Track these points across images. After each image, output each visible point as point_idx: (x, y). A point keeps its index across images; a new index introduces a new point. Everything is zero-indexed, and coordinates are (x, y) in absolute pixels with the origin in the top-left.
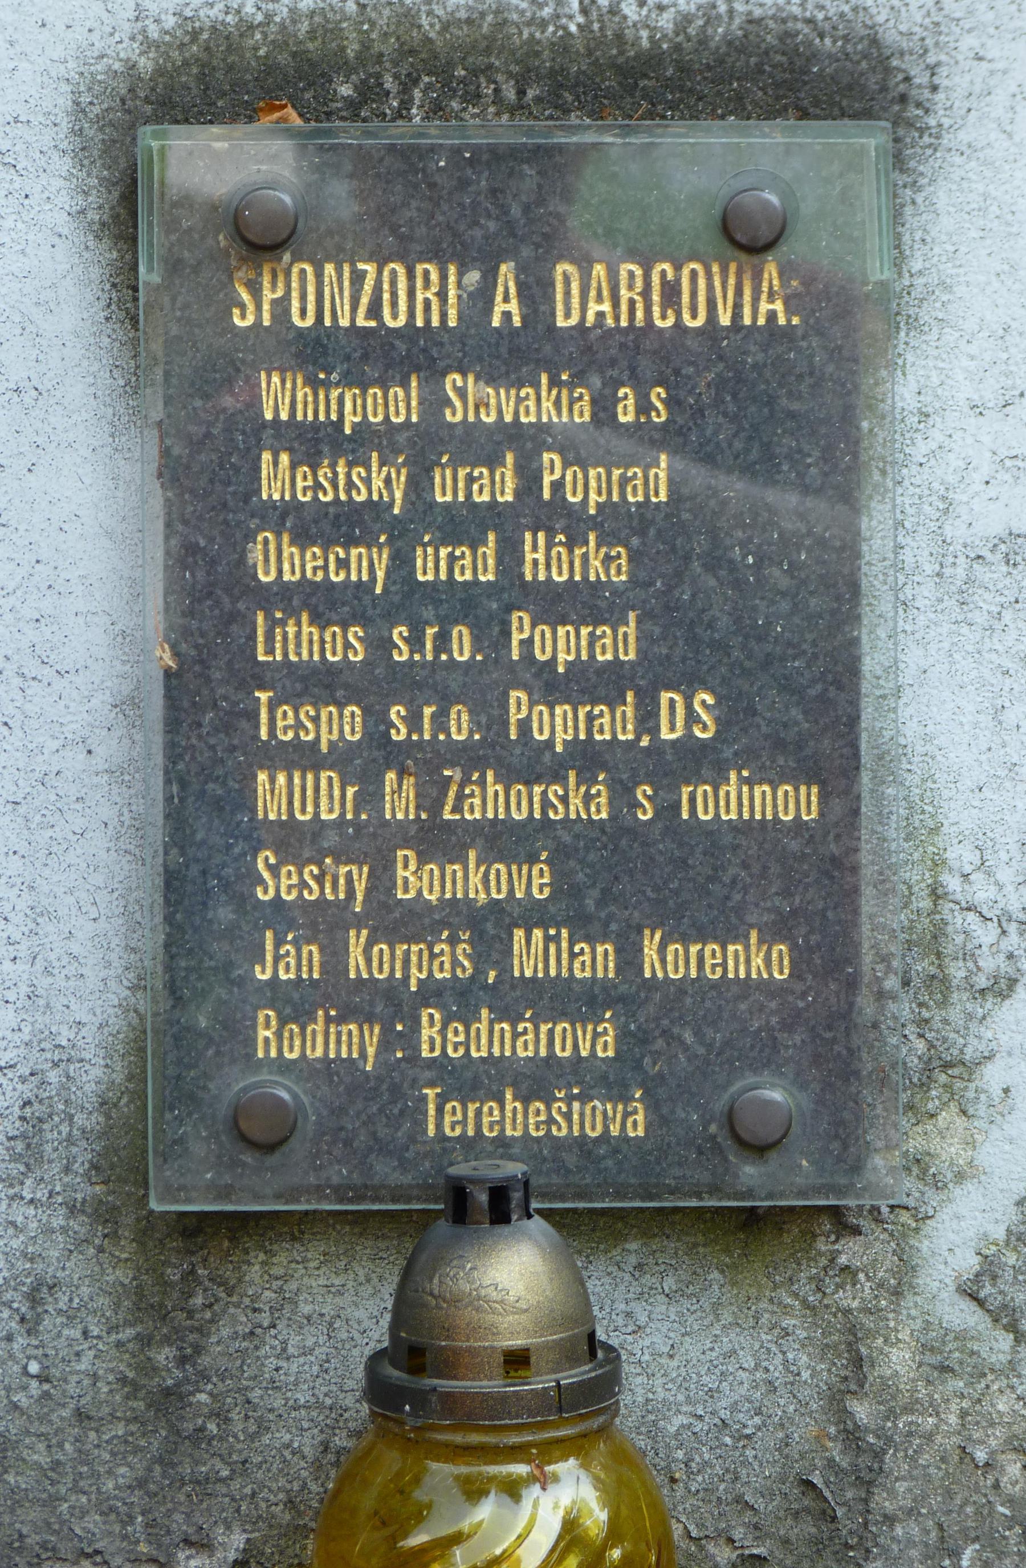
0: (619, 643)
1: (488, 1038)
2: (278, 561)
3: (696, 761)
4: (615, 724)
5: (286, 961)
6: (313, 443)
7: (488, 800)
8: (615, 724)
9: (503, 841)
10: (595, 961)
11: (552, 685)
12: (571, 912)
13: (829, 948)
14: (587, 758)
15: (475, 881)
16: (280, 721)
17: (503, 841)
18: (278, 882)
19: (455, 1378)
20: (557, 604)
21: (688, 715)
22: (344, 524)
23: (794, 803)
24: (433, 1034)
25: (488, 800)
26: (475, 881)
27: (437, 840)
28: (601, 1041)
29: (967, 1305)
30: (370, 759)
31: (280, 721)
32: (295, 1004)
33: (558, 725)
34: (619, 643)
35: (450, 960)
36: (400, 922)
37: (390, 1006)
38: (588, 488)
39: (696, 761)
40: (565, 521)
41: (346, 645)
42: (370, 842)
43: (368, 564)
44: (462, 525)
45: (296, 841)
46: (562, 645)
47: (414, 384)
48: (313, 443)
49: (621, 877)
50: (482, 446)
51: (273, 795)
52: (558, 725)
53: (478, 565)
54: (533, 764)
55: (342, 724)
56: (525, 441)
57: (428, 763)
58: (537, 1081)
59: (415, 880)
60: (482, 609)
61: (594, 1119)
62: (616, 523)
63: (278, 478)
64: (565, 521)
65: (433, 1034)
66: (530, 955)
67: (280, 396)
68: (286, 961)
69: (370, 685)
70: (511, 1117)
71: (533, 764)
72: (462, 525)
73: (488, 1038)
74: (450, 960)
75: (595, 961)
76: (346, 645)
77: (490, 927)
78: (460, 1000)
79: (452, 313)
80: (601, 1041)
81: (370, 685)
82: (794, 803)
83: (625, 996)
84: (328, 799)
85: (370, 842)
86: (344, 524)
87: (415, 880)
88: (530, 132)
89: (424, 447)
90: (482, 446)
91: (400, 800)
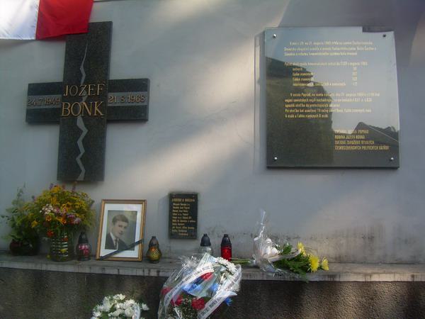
3: (189, 220)
5: (174, 227)
6: (175, 206)
7: (182, 221)
19: (135, 223)
21: (190, 218)
22: (176, 209)
24: (180, 231)
25: (182, 221)
27: (180, 223)
28: (186, 231)
29: (203, 235)
36: (178, 226)
39: (189, 220)
42: (177, 223)
48: (175, 206)
49: (187, 224)
51: (173, 221)
55: (176, 218)
65: (180, 231)
66: (183, 227)
67: (174, 204)
68: (174, 227)
80: (186, 231)
86: (176, 209)
88: (214, 303)
89: (179, 206)
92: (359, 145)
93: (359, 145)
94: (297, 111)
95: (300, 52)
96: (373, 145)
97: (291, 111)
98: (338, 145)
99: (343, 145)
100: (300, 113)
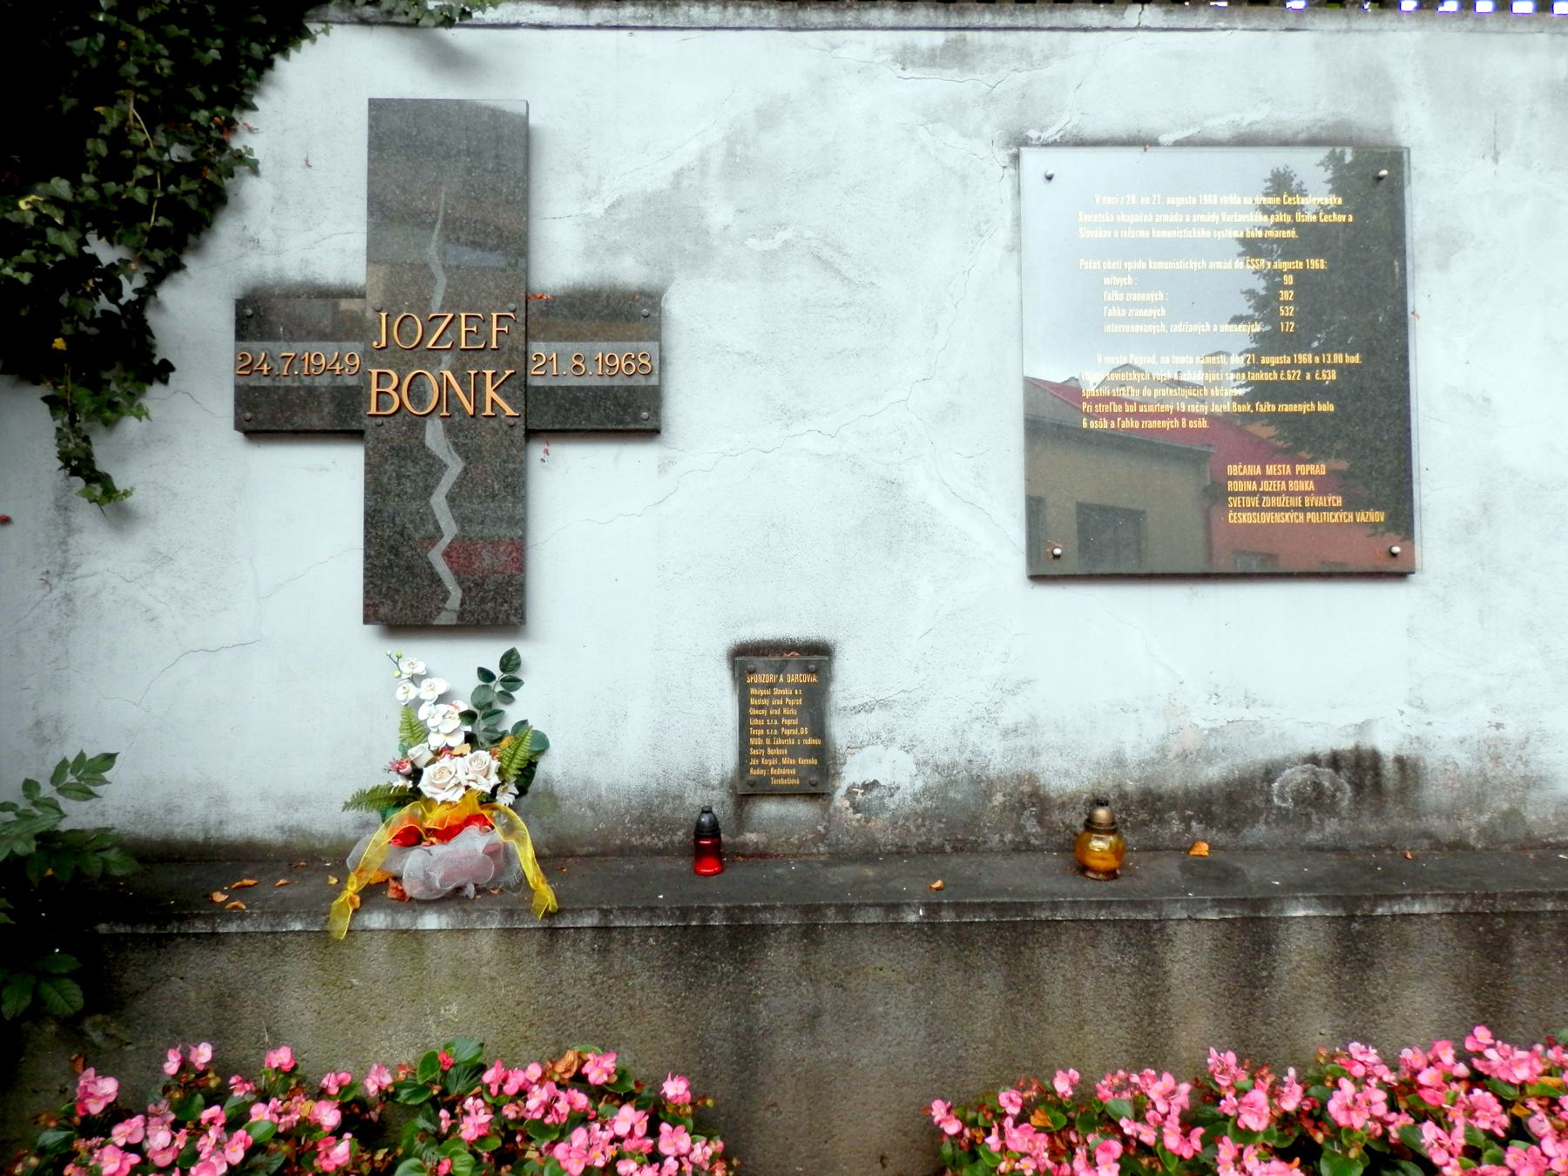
0: (795, 722)
1: (779, 772)
2: (753, 712)
3: (805, 736)
4: (795, 732)
5: (754, 762)
7: (779, 742)
8: (795, 732)
9: (781, 747)
10: (793, 762)
11: (786, 727)
12: (790, 756)
13: (822, 762)
14: (792, 736)
15: (778, 752)
16: (753, 732)
17: (781, 747)
18: (753, 752)
20: (787, 717)
21: (804, 731)
22: (761, 707)
23: (817, 742)
25: (779, 742)
26: (778, 752)
27: (773, 747)
28: (793, 772)
30: (764, 737)
31: (753, 732)
32: (755, 767)
33: (788, 732)
34: (795, 722)
35: (774, 762)
36: (768, 757)
37: (767, 767)
38: (792, 702)
39: (805, 736)
40: (788, 706)
41: (761, 722)
42: (764, 747)
43: (764, 712)
44: (776, 707)
45: (755, 747)
46: (788, 722)
47: (1341, 218)
50: (778, 697)
51: (752, 741)
52: (788, 732)
53: (778, 712)
54: (784, 737)
55: (761, 732)
56: (784, 697)
57: (772, 737)
58: (786, 777)
59: (770, 752)
60: (779, 718)
61: (792, 781)
62: (795, 707)
63: (752, 701)
64: (788, 706)
66: (784, 761)
68: (754, 762)
69: (765, 727)
70: (782, 782)
71: (784, 737)
72: (776, 707)
73: (779, 772)
74: (774, 762)
75: (793, 762)
76: (761, 722)
77: (780, 757)
78: (775, 767)
79: (1234, 200)
81: (765, 727)
82: (817, 742)
83: (797, 766)
84: (759, 742)
85: (764, 747)
86: (761, 707)
87: (770, 752)
90: (778, 697)
91: (768, 742)
92: (1296, 509)
93: (1296, 509)
94: (1118, 408)
95: (1126, 226)
96: (1337, 509)
97: (1100, 408)
98: (1236, 510)
99: (1252, 509)
100: (1125, 415)
